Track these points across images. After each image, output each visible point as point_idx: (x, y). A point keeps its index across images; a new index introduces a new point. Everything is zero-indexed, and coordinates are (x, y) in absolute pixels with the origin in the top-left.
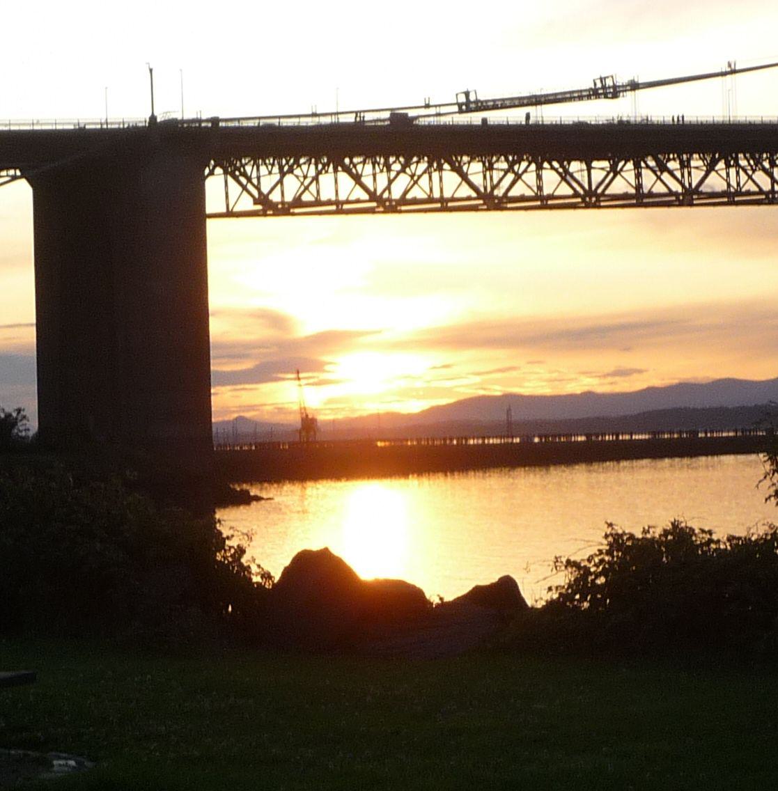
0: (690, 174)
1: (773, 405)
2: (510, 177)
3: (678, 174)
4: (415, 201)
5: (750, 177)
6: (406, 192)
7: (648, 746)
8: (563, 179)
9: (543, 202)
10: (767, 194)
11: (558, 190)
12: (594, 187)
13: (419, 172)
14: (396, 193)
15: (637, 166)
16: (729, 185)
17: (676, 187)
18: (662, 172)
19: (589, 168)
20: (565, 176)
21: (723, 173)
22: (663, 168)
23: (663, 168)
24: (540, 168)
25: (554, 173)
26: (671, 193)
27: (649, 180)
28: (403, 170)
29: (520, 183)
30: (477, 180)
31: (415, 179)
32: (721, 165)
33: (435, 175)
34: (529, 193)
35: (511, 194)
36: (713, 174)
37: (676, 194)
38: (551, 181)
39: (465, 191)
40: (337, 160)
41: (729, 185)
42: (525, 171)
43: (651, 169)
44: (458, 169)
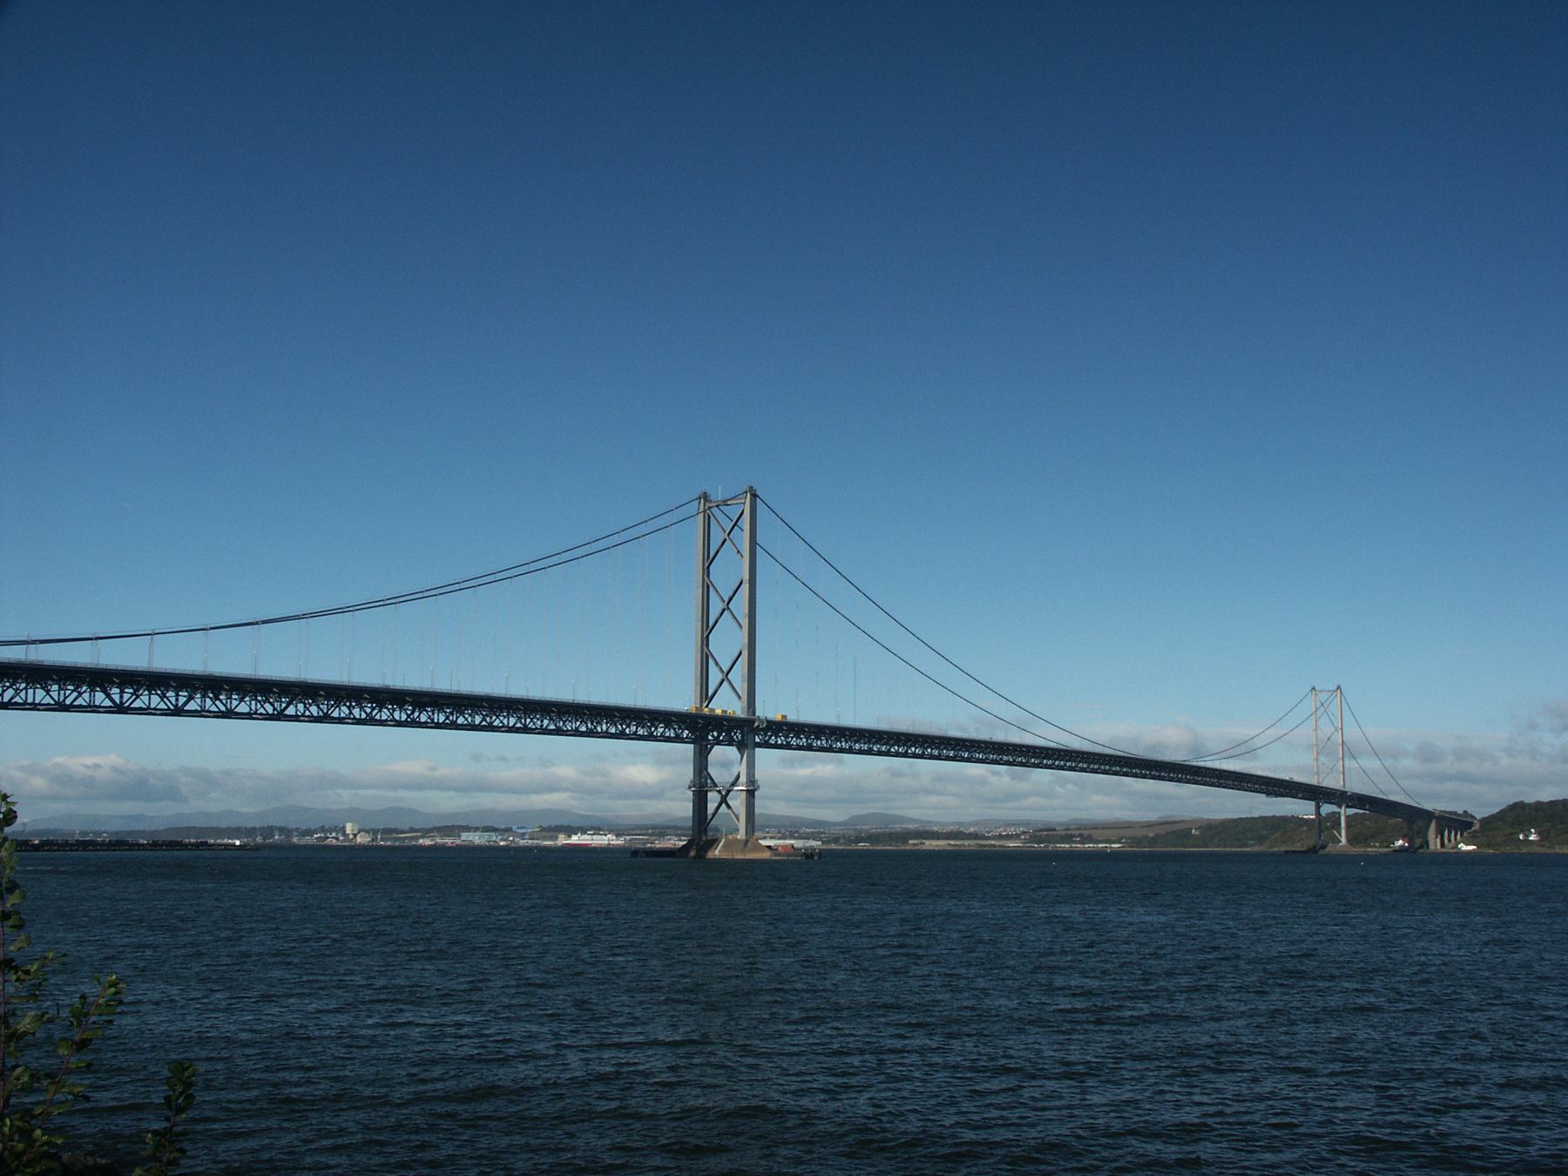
0: (231, 703)
1: (260, 860)
2: (75, 694)
3: (224, 701)
4: (16, 703)
5: (262, 706)
6: (12, 698)
7: (1445, 932)
8: (162, 700)
9: (92, 708)
10: (271, 715)
11: (135, 703)
12: (57, 700)
13: (21, 688)
14: (68, 702)
15: (150, 694)
16: (251, 709)
17: (223, 709)
18: (216, 700)
19: (177, 695)
20: (163, 697)
21: (248, 703)
22: (267, 701)
23: (165, 696)
24: (150, 694)
25: (157, 696)
26: (220, 711)
27: (356, 712)
28: (11, 687)
29: (80, 698)
30: (117, 698)
31: (80, 694)
32: (247, 699)
33: (31, 691)
34: (85, 704)
35: (132, 706)
36: (243, 703)
37: (222, 712)
38: (100, 698)
39: (108, 703)
40: (441, 710)
41: (251, 709)
42: (85, 692)
43: (211, 698)
44: (104, 691)
